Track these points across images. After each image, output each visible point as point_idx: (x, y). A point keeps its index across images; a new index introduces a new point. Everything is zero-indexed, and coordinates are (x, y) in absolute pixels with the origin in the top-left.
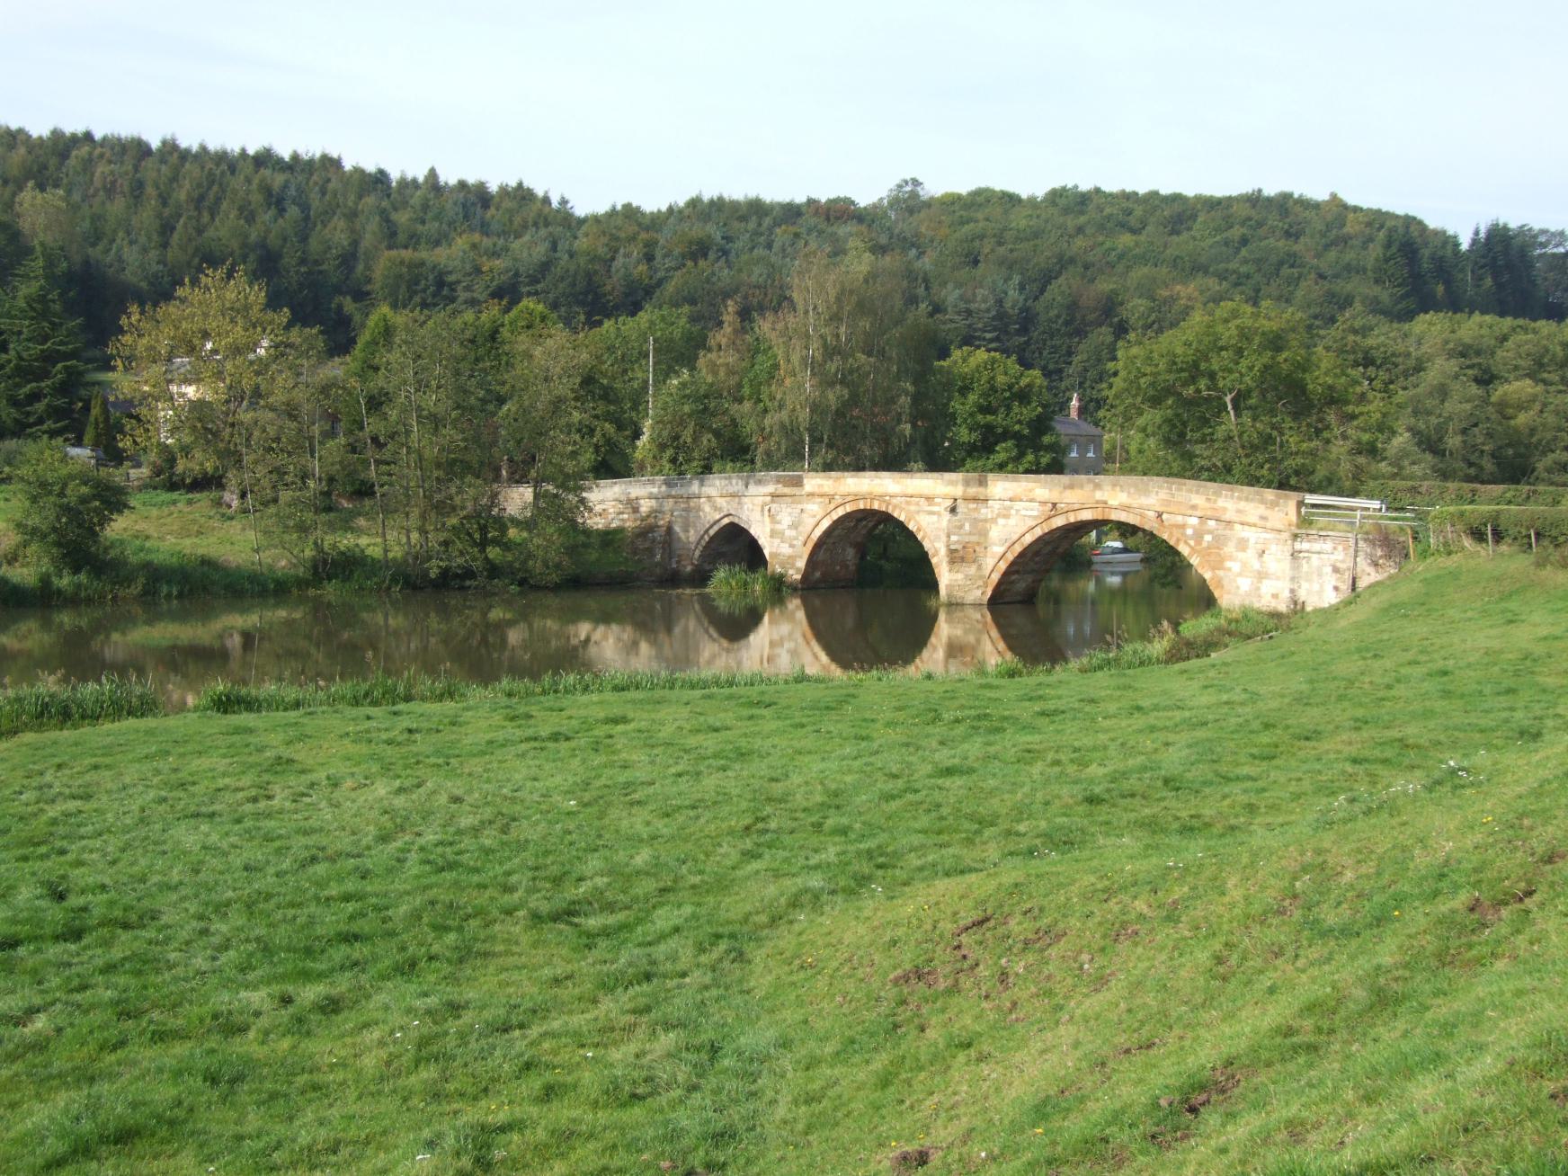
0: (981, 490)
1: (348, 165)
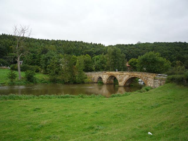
0: (20, 70)
1: (84, 42)
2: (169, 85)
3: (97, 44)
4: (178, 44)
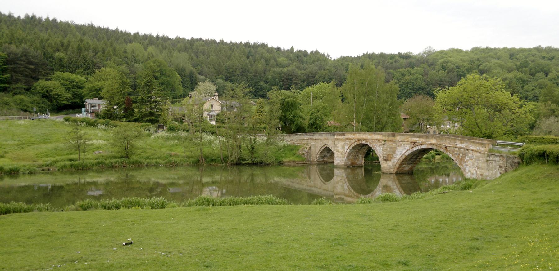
2: (523, 170)
3: (309, 52)
4: (544, 54)
